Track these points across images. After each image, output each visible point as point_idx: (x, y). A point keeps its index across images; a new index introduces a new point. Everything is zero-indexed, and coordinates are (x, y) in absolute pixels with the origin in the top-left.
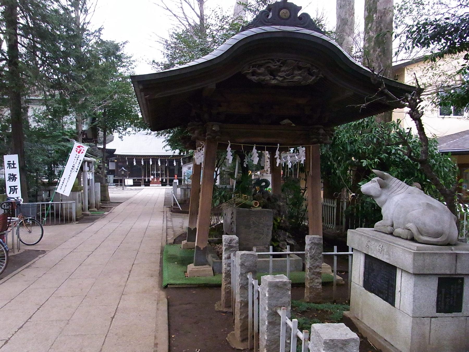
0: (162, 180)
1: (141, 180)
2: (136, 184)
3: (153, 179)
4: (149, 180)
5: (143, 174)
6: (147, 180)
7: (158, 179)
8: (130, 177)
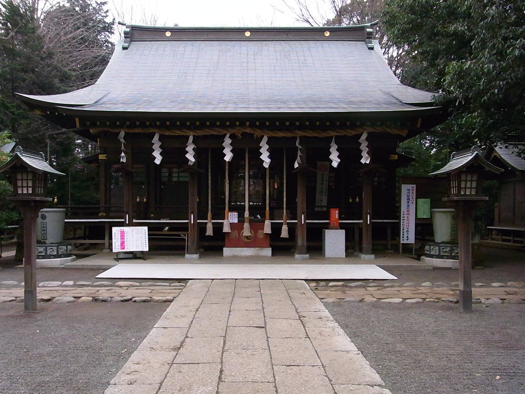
0: (276, 229)
1: (184, 228)
2: (163, 246)
3: (236, 227)
4: (218, 228)
5: (194, 200)
6: (210, 232)
7: (257, 225)
8: (138, 215)
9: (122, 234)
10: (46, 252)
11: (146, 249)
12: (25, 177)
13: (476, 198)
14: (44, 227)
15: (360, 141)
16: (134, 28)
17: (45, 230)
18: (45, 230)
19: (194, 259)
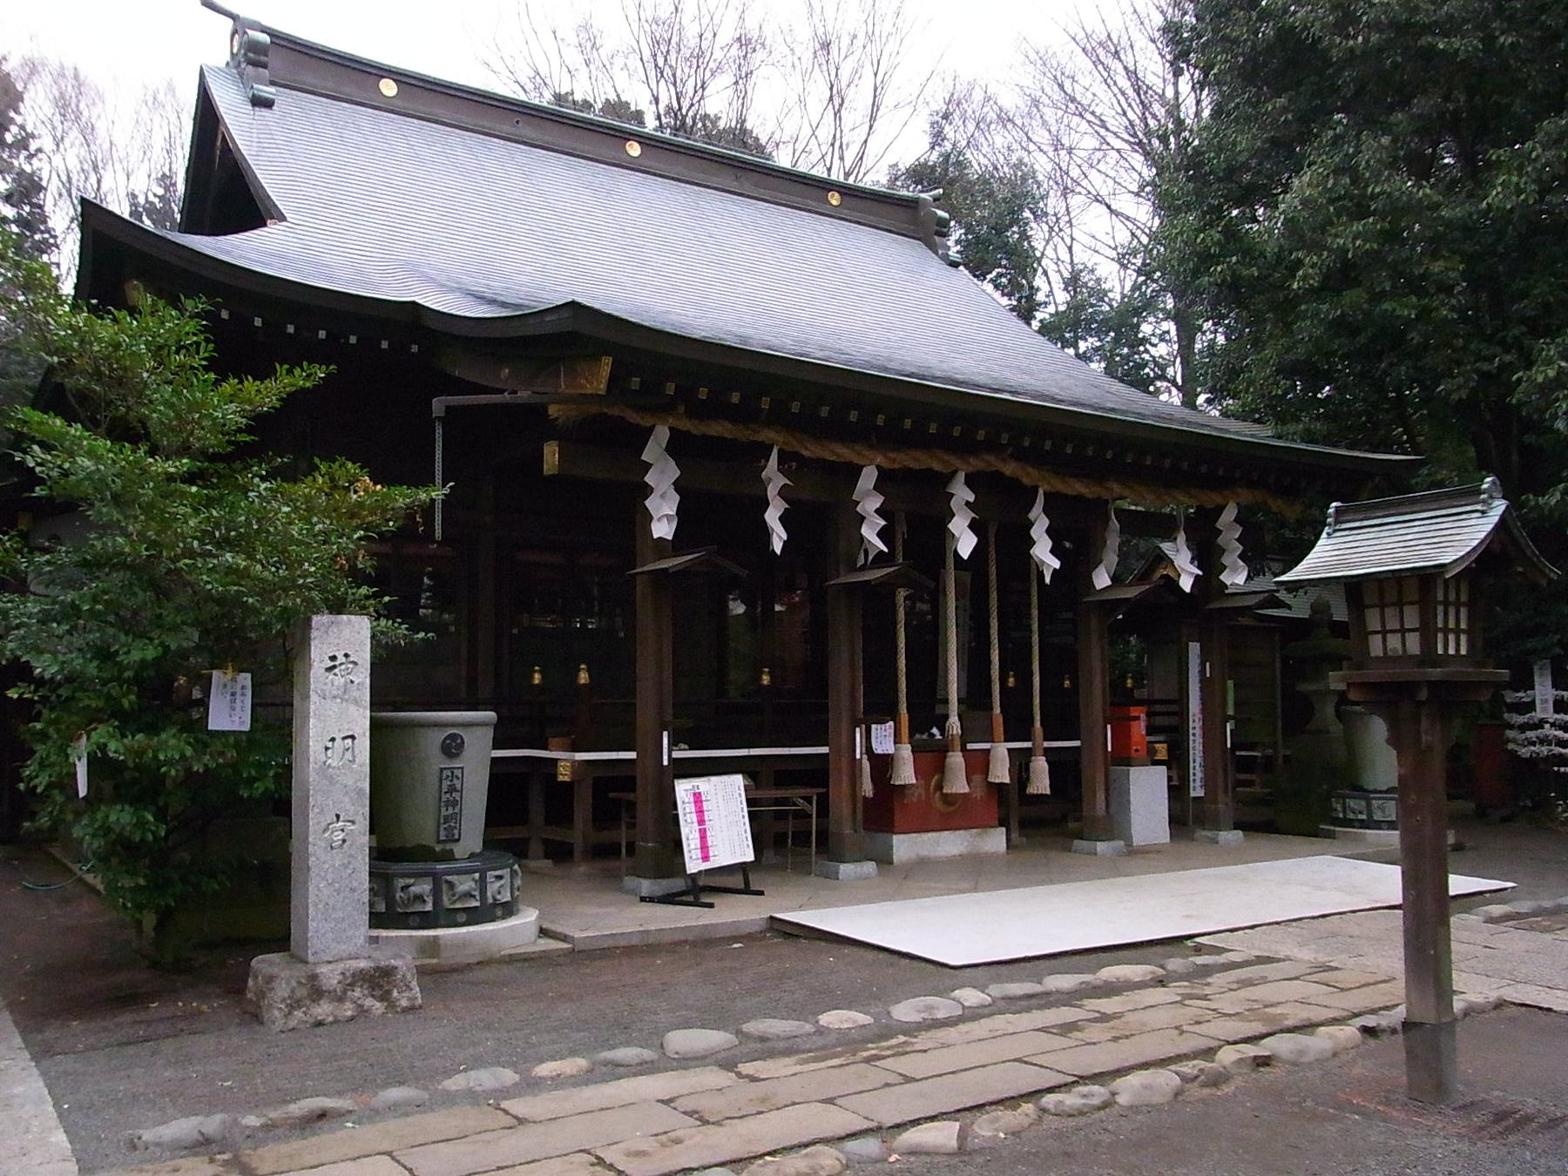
9: (698, 798)
10: (483, 892)
11: (749, 856)
12: (1393, 624)
13: (1471, 673)
14: (452, 789)
15: (1219, 525)
16: (284, 43)
17: (454, 803)
18: (454, 803)
19: (867, 878)
